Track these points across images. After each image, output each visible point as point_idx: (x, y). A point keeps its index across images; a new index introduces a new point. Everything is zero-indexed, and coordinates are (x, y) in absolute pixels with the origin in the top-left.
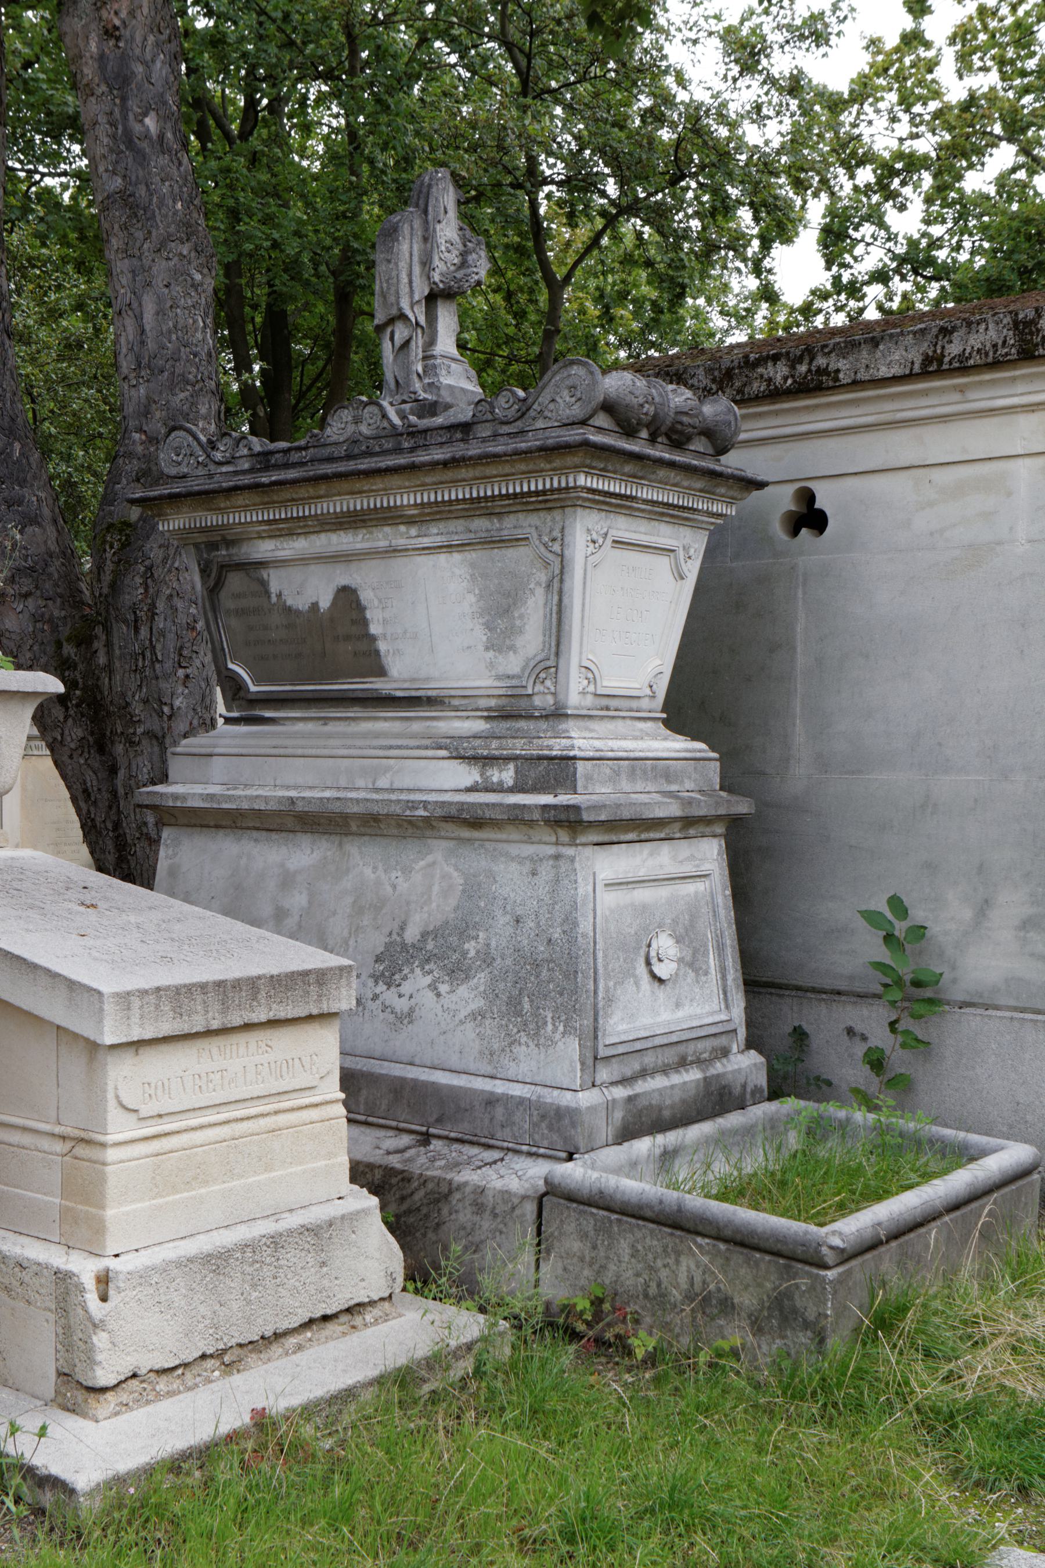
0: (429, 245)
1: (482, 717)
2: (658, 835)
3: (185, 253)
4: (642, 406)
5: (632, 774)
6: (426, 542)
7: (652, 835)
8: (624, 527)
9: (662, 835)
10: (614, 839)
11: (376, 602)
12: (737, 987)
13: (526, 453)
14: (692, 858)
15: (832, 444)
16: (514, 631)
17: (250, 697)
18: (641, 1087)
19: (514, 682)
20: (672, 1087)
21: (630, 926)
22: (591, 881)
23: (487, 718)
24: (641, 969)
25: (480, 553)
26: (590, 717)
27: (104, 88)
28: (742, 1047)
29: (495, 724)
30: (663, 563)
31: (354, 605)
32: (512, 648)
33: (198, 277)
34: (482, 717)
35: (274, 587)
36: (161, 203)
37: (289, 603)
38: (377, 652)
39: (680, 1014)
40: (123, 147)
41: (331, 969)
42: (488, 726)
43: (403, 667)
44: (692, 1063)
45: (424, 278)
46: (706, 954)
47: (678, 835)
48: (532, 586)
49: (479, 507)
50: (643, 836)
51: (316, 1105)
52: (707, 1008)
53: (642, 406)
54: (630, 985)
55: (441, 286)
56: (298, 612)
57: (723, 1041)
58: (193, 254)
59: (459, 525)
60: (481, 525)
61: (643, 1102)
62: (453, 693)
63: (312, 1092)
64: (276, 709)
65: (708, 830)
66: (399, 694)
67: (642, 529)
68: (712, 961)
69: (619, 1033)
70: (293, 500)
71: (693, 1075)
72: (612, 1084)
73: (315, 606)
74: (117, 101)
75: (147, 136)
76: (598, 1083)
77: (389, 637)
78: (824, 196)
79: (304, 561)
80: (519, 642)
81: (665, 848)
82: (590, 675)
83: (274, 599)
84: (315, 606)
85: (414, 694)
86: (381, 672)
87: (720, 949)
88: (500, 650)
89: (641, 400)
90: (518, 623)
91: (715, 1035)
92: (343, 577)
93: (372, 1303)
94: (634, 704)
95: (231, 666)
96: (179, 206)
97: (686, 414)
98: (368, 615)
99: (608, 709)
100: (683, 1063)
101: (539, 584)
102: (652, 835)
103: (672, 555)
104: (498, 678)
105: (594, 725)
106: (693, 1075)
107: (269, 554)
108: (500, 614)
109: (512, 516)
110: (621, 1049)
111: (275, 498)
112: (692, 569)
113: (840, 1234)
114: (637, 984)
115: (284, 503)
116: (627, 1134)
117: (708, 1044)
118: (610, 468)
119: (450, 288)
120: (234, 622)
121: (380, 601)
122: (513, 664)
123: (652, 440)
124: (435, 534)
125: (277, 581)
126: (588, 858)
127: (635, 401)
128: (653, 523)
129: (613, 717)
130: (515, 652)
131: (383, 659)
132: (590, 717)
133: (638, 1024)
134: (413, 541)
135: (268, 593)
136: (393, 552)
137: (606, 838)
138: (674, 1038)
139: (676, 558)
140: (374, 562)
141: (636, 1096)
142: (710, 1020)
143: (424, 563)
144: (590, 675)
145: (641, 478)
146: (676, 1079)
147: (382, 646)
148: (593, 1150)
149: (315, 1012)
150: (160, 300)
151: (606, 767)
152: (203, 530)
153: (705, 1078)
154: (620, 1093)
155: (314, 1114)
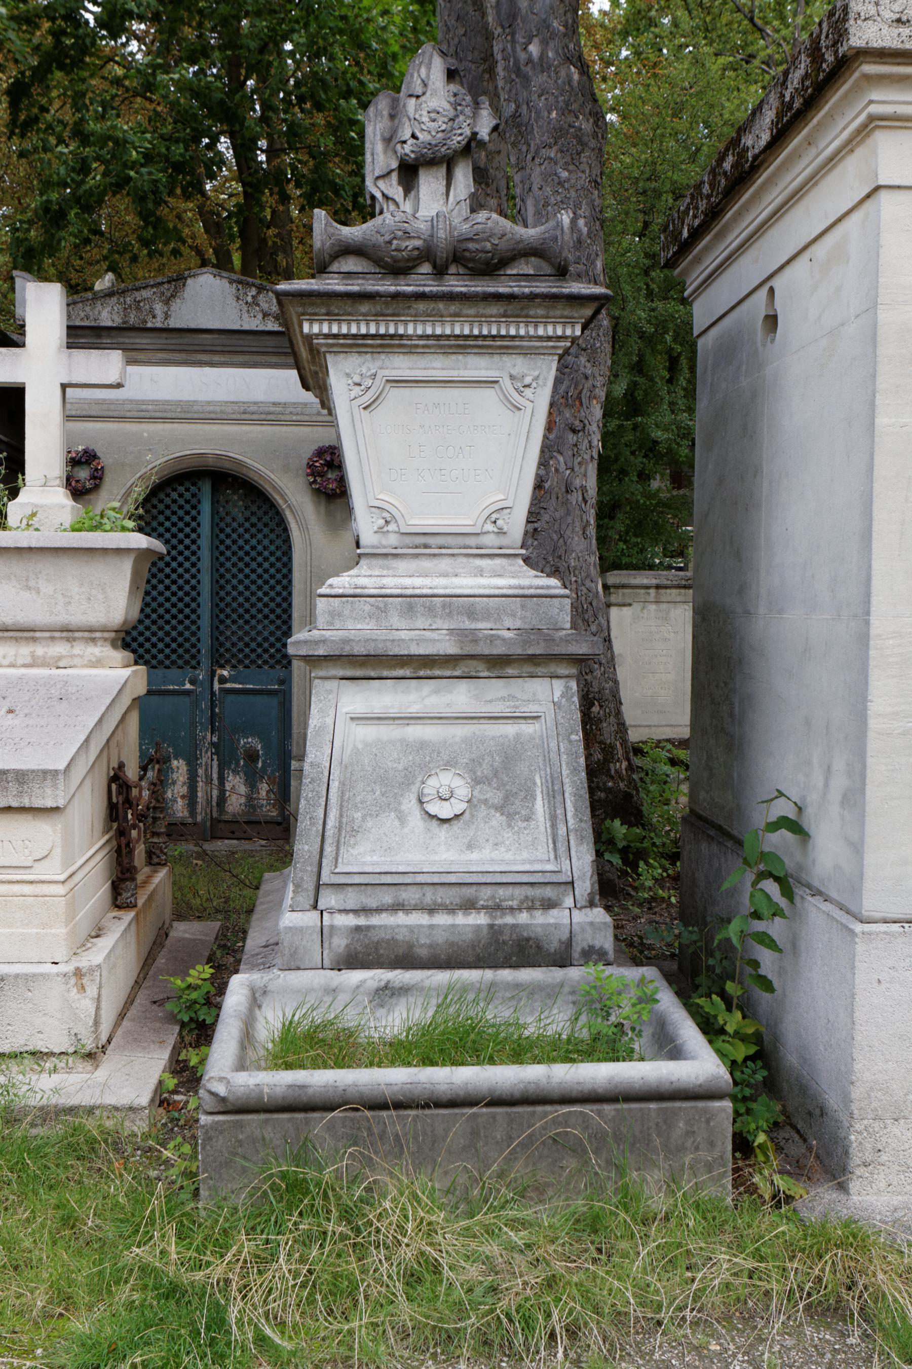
0: (396, 121)
2: (448, 673)
3: (552, 155)
4: (390, 242)
5: (409, 611)
7: (437, 672)
8: (401, 365)
9: (457, 673)
10: (373, 674)
12: (582, 839)
14: (512, 697)
15: (775, 233)
18: (375, 920)
20: (431, 927)
21: (398, 760)
22: (332, 713)
24: (409, 803)
26: (395, 556)
27: (499, 30)
28: (582, 902)
30: (489, 394)
33: (565, 174)
36: (538, 117)
39: (474, 856)
40: (514, 76)
41: (33, 771)
44: (484, 907)
45: (390, 153)
46: (530, 797)
47: (486, 674)
50: (421, 673)
51: (32, 882)
52: (525, 855)
53: (390, 242)
54: (389, 820)
55: (413, 156)
57: (549, 892)
58: (559, 155)
61: (375, 936)
63: (28, 871)
65: (540, 670)
67: (437, 364)
68: (540, 807)
69: (364, 864)
71: (480, 919)
72: (340, 911)
74: (509, 38)
75: (530, 61)
76: (322, 905)
81: (463, 686)
82: (386, 515)
87: (554, 794)
89: (387, 238)
91: (532, 884)
93: (52, 1054)
94: (472, 541)
96: (554, 115)
97: (471, 239)
99: (426, 546)
100: (469, 906)
102: (437, 672)
103: (496, 386)
105: (394, 563)
106: (480, 919)
110: (357, 879)
112: (543, 397)
113: (229, 1082)
114: (402, 819)
116: (351, 961)
117: (519, 892)
119: (423, 155)
123: (440, 272)
126: (330, 692)
127: (381, 239)
128: (453, 357)
129: (434, 555)
132: (395, 556)
133: (398, 858)
137: (359, 673)
138: (452, 879)
139: (501, 389)
141: (368, 928)
142: (527, 867)
144: (386, 515)
145: (398, 315)
146: (461, 919)
148: (299, 969)
149: (15, 804)
150: (537, 201)
151: (364, 605)
153: (491, 926)
154: (351, 921)
155: (27, 889)
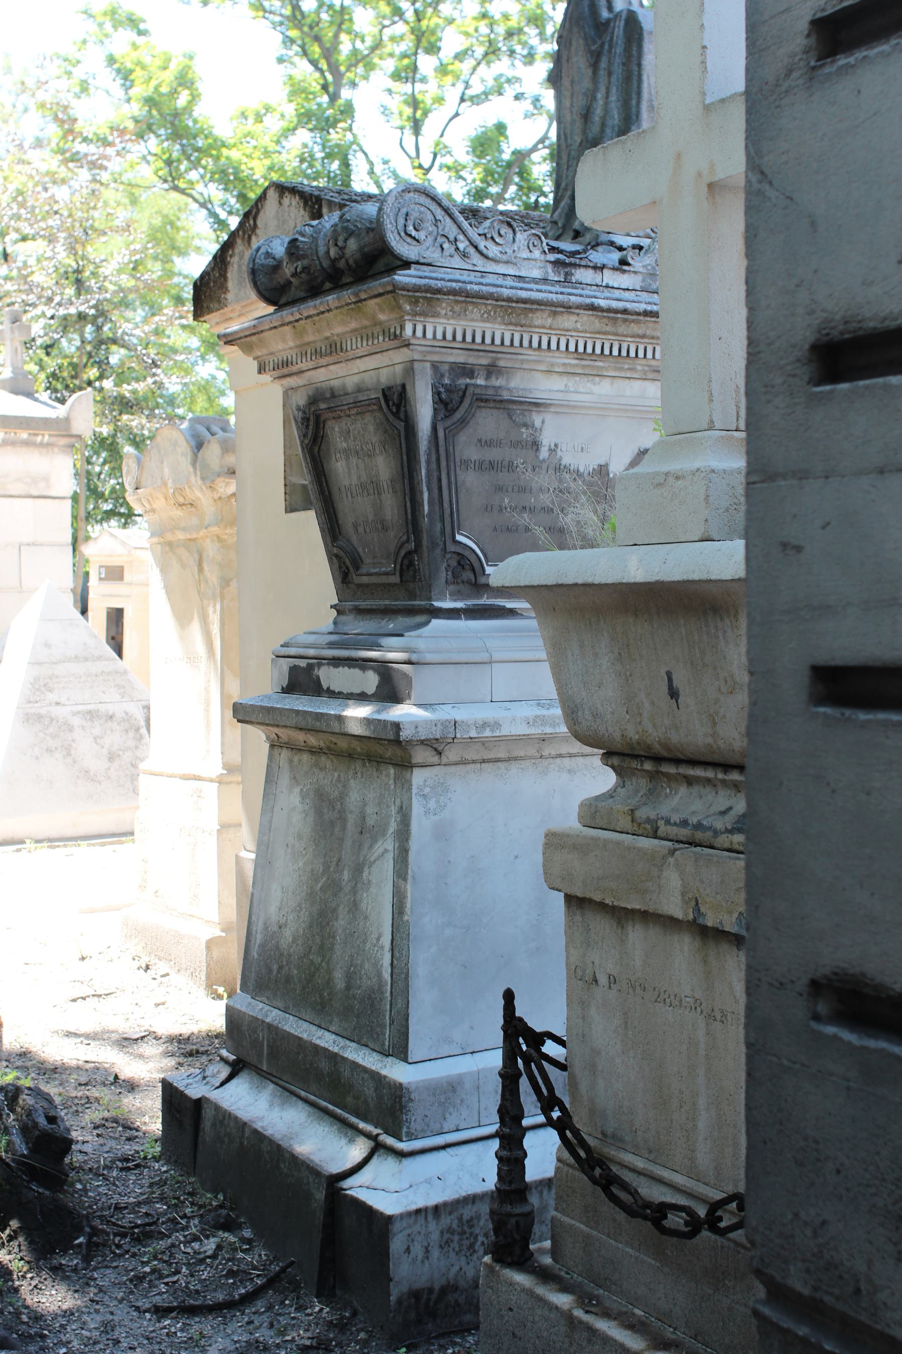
35: (547, 439)
125: (551, 431)
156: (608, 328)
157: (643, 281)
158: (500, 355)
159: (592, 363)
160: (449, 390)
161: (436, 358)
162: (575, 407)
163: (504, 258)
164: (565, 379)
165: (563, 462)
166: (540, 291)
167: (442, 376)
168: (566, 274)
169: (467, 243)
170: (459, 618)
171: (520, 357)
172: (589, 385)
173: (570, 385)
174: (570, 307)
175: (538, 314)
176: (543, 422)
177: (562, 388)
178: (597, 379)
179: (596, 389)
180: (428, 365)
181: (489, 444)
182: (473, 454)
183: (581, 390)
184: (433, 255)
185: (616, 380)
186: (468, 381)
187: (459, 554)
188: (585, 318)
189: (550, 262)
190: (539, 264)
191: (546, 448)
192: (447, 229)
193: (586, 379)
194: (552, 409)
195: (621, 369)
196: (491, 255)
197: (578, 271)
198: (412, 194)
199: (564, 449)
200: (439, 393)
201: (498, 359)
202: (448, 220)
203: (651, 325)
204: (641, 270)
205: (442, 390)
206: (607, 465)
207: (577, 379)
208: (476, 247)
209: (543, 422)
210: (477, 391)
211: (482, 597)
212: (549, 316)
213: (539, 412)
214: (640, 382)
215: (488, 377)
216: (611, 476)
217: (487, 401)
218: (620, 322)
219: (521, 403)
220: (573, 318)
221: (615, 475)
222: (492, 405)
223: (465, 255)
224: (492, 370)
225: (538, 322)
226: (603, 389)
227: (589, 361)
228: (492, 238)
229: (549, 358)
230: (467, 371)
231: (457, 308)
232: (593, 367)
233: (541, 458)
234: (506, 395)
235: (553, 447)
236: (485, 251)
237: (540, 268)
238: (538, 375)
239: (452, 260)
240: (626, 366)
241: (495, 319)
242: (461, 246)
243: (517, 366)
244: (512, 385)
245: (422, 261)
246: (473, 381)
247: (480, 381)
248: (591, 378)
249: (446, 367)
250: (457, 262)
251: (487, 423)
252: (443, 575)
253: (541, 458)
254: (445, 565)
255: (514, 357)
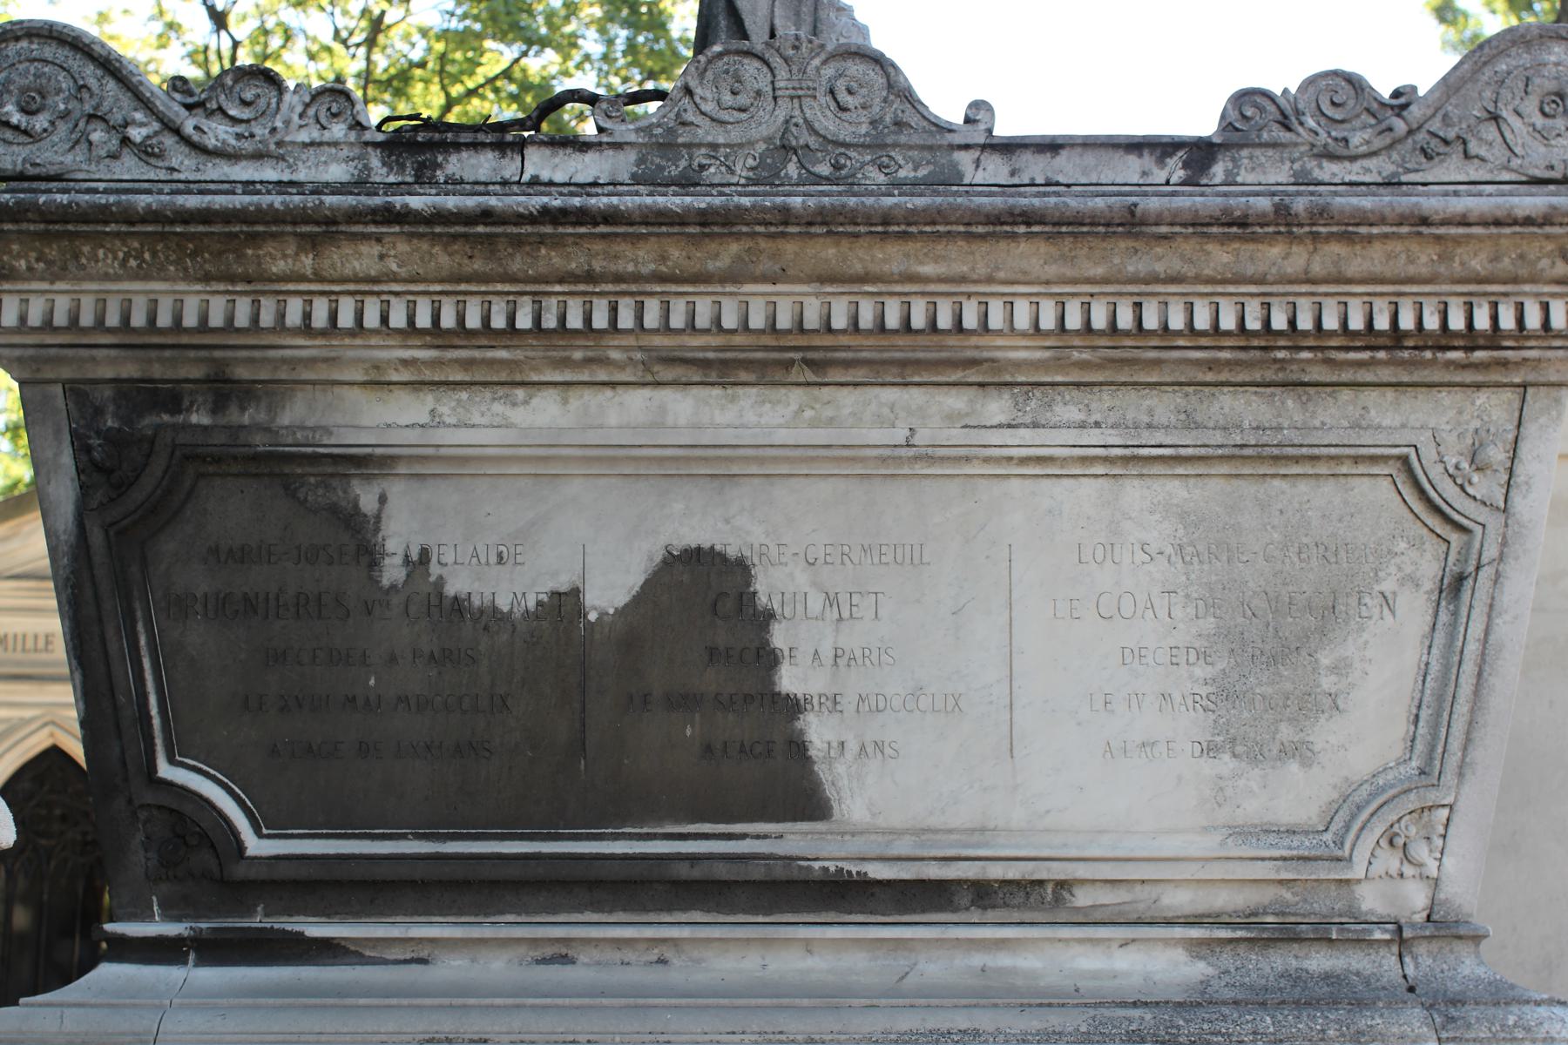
1: (1178, 942)
6: (1055, 441)
11: (816, 603)
13: (1528, 221)
16: (1311, 704)
17: (240, 872)
19: (1305, 846)
23: (1197, 948)
25: (1215, 485)
29: (1227, 959)
31: (728, 605)
32: (1300, 752)
34: (1178, 942)
35: (399, 536)
37: (456, 585)
38: (798, 748)
42: (1200, 969)
43: (883, 792)
48: (1388, 586)
49: (1268, 357)
56: (491, 618)
59: (1164, 406)
60: (1243, 411)
62: (1081, 871)
64: (327, 912)
66: (878, 872)
70: (590, 277)
73: (566, 604)
77: (848, 702)
78: (499, 83)
79: (544, 464)
80: (1325, 733)
83: (392, 572)
84: (566, 604)
85: (934, 872)
86: (807, 802)
88: (1255, 756)
90: (1327, 682)
92: (695, 523)
95: (165, 770)
98: (779, 637)
101: (1413, 581)
104: (1241, 832)
107: (412, 437)
108: (1265, 659)
109: (1346, 394)
111: (517, 265)
115: (537, 285)
118: (476, 419)
120: (197, 636)
121: (831, 600)
122: (1297, 796)
124: (1070, 422)
125: (404, 522)
130: (1306, 763)
131: (821, 770)
134: (995, 437)
135: (370, 555)
136: (908, 461)
140: (824, 488)
143: (1022, 504)
147: (818, 731)
152: (130, 340)
156: (478, 265)
157: (641, 161)
158: (229, 354)
159: (477, 354)
160: (115, 440)
161: (67, 373)
162: (465, 460)
163: (247, 146)
164: (429, 399)
165: (451, 590)
166: (249, 186)
167: (99, 412)
168: (420, 169)
169: (156, 126)
170: (180, 960)
171: (272, 353)
172: (498, 407)
173: (444, 410)
174: (335, 222)
175: (270, 247)
176: (383, 499)
177: (424, 418)
178: (520, 393)
179: (518, 415)
180: (58, 389)
181: (242, 556)
182: (200, 581)
183: (477, 419)
184: (72, 160)
185: (574, 393)
186: (166, 418)
187: (172, 811)
188: (403, 247)
189: (376, 145)
190: (345, 152)
191: (398, 560)
192: (106, 106)
193: (487, 394)
194: (402, 469)
195: (566, 363)
196: (211, 142)
197: (453, 158)
198: (24, 44)
199: (449, 558)
200: (88, 449)
201: (225, 363)
202: (111, 85)
203: (598, 246)
204: (632, 138)
205: (95, 442)
206: (575, 593)
207: (464, 395)
208: (177, 131)
209: (383, 499)
210: (182, 438)
211: (249, 912)
212: (301, 249)
213: (369, 478)
214: (646, 392)
215: (218, 407)
216: (592, 617)
217: (218, 460)
218: (502, 245)
219: (315, 459)
220: (371, 250)
221: (603, 614)
222: (235, 469)
223: (146, 152)
224: (224, 389)
225: (279, 267)
226: (543, 414)
227: (475, 359)
228: (220, 109)
229: (352, 349)
230: (170, 398)
231: (52, 252)
232: (492, 363)
233: (385, 582)
234: (260, 443)
235: (415, 556)
236: (196, 137)
237: (348, 160)
238: (355, 394)
239: (116, 165)
240: (578, 355)
241: (162, 268)
242: (136, 134)
243: (283, 376)
244: (285, 419)
245: (31, 171)
246: (180, 419)
247: (199, 418)
248: (501, 391)
249: (108, 392)
250: (129, 168)
251: (230, 511)
252: (139, 859)
253: (385, 582)
254: (140, 836)
255: (257, 354)
